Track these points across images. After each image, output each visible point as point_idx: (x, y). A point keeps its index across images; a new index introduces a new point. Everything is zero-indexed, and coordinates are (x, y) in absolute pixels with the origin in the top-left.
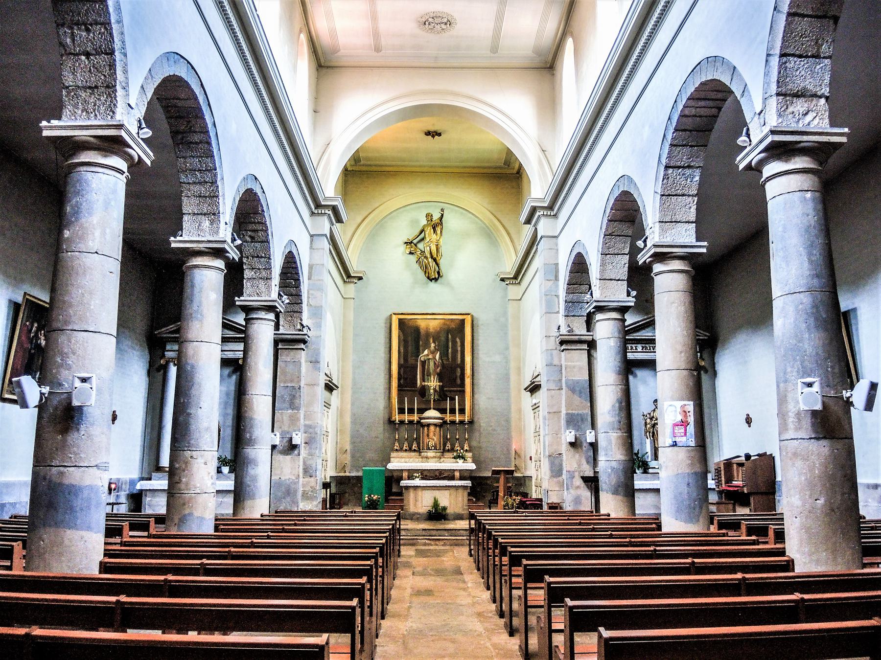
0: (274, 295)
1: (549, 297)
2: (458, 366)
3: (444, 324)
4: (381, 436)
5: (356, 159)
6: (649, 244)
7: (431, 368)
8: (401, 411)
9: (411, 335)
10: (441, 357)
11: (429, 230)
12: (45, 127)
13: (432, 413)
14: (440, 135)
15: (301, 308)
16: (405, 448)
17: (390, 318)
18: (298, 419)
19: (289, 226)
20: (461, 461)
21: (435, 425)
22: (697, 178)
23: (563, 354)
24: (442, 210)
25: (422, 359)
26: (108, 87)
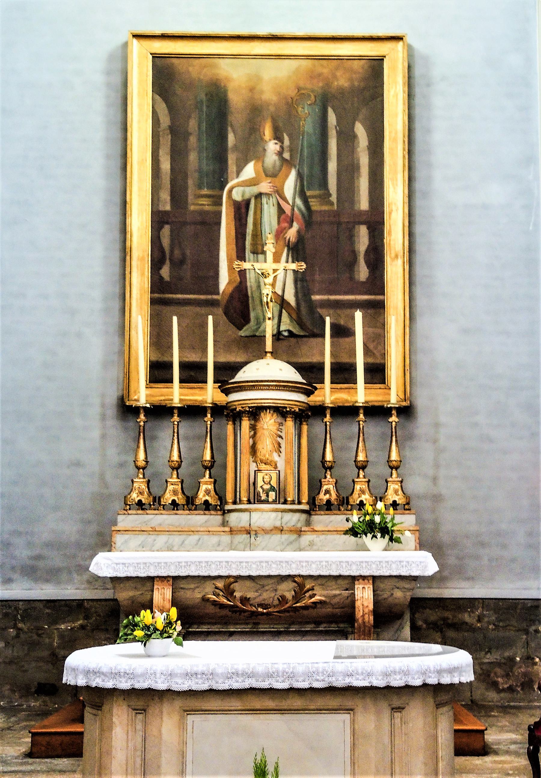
2: (360, 218)
3: (312, 76)
4: (93, 462)
8: (159, 372)
9: (196, 113)
16: (168, 498)
17: (123, 54)
20: (376, 545)
21: (281, 411)
25: (237, 195)
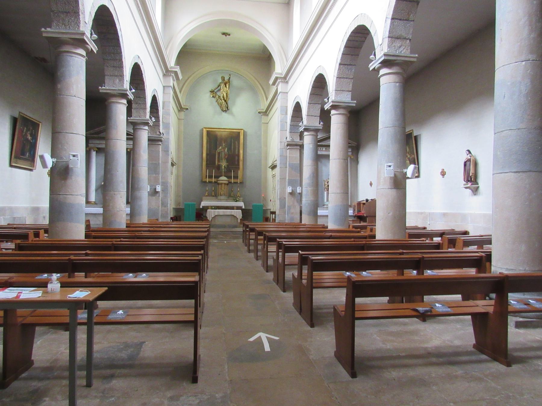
0: (148, 117)
1: (283, 123)
5: (185, 46)
6: (330, 100)
7: (223, 156)
10: (228, 151)
11: (222, 85)
12: (44, 31)
13: (223, 178)
14: (229, 35)
15: (159, 124)
17: (202, 130)
18: (159, 179)
19: (153, 83)
21: (225, 184)
22: (353, 70)
23: (288, 151)
24: (230, 75)
26: (75, 12)
